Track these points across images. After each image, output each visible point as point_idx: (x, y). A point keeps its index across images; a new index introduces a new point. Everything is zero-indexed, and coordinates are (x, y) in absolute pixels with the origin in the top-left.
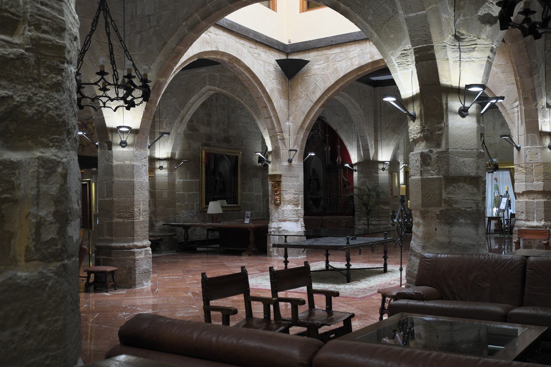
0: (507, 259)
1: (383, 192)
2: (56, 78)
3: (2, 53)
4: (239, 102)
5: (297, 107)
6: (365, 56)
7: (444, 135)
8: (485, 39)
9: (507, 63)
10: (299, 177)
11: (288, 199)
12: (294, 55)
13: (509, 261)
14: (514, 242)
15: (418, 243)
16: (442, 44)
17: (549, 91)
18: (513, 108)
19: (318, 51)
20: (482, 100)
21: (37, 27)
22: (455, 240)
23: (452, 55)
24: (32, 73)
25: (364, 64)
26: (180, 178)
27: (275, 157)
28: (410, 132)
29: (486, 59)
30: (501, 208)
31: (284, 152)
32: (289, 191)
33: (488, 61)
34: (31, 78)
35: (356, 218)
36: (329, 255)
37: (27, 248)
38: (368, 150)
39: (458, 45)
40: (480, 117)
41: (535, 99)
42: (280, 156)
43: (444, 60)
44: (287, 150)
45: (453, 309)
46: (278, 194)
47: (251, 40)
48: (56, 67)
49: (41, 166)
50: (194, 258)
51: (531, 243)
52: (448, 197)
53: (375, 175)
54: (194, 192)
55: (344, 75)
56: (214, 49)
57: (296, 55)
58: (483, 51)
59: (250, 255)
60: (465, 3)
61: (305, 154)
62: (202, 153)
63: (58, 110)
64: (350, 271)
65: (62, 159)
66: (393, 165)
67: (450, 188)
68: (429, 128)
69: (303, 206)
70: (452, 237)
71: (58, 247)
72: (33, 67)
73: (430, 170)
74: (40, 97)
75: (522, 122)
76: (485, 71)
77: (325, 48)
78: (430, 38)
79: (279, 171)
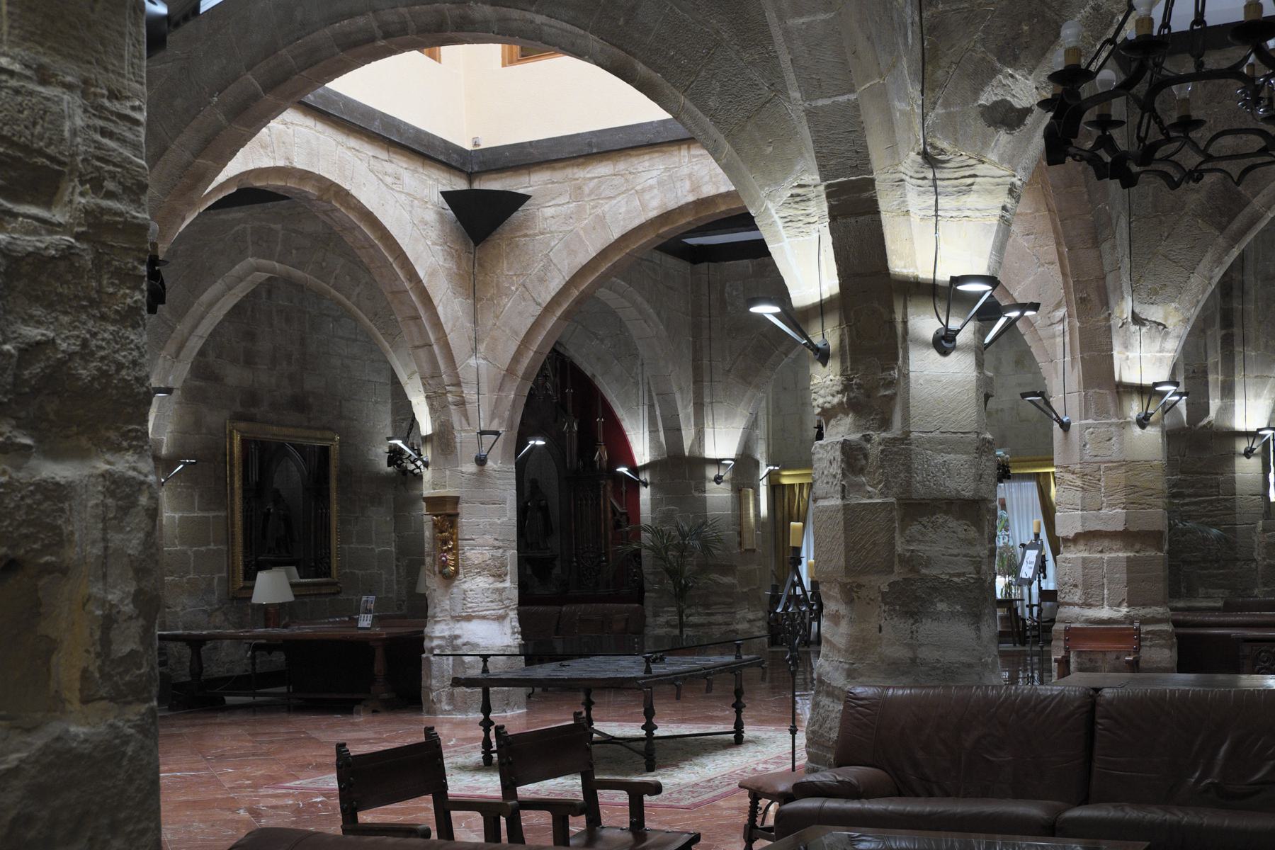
0: (1052, 695)
1: (720, 540)
2: (132, 298)
3: (35, 246)
4: (339, 303)
5: (497, 317)
6: (678, 184)
7: (898, 399)
8: (994, 164)
9: (1038, 210)
10: (504, 502)
11: (476, 562)
12: (489, 180)
13: (1057, 699)
14: (1056, 660)
15: (836, 664)
16: (894, 176)
17: (1138, 281)
18: (1052, 324)
19: (554, 169)
20: (989, 312)
21: (96, 185)
22: (926, 654)
23: (918, 201)
24: (87, 287)
25: (675, 206)
26: (174, 510)
27: (443, 450)
28: (816, 390)
29: (999, 212)
30: (1023, 575)
31: (465, 437)
32: (480, 541)
33: (1003, 216)
34: (85, 298)
35: (649, 611)
36: (593, 703)
37: (85, 675)
38: (679, 430)
39: (930, 176)
40: (980, 351)
41: (1105, 303)
42: (455, 447)
43: (898, 215)
44: (473, 431)
45: (930, 814)
46: (450, 550)
47: (374, 138)
48: (131, 272)
49: (110, 493)
50: (222, 724)
51: (1096, 662)
52: (908, 550)
53: (696, 494)
54: (212, 547)
55: (623, 236)
56: (281, 163)
57: (495, 179)
58: (990, 192)
59: (375, 711)
60: (948, 72)
61: (521, 443)
62: (232, 439)
63: (137, 368)
64: (656, 741)
65: (146, 476)
66: (744, 464)
67: (915, 528)
68: (862, 382)
69: (516, 579)
70: (920, 645)
71: (142, 671)
72: (90, 275)
73: (864, 484)
74: (103, 340)
75: (1073, 359)
76: (994, 242)
77: (573, 162)
78: (866, 160)
79: (451, 486)
